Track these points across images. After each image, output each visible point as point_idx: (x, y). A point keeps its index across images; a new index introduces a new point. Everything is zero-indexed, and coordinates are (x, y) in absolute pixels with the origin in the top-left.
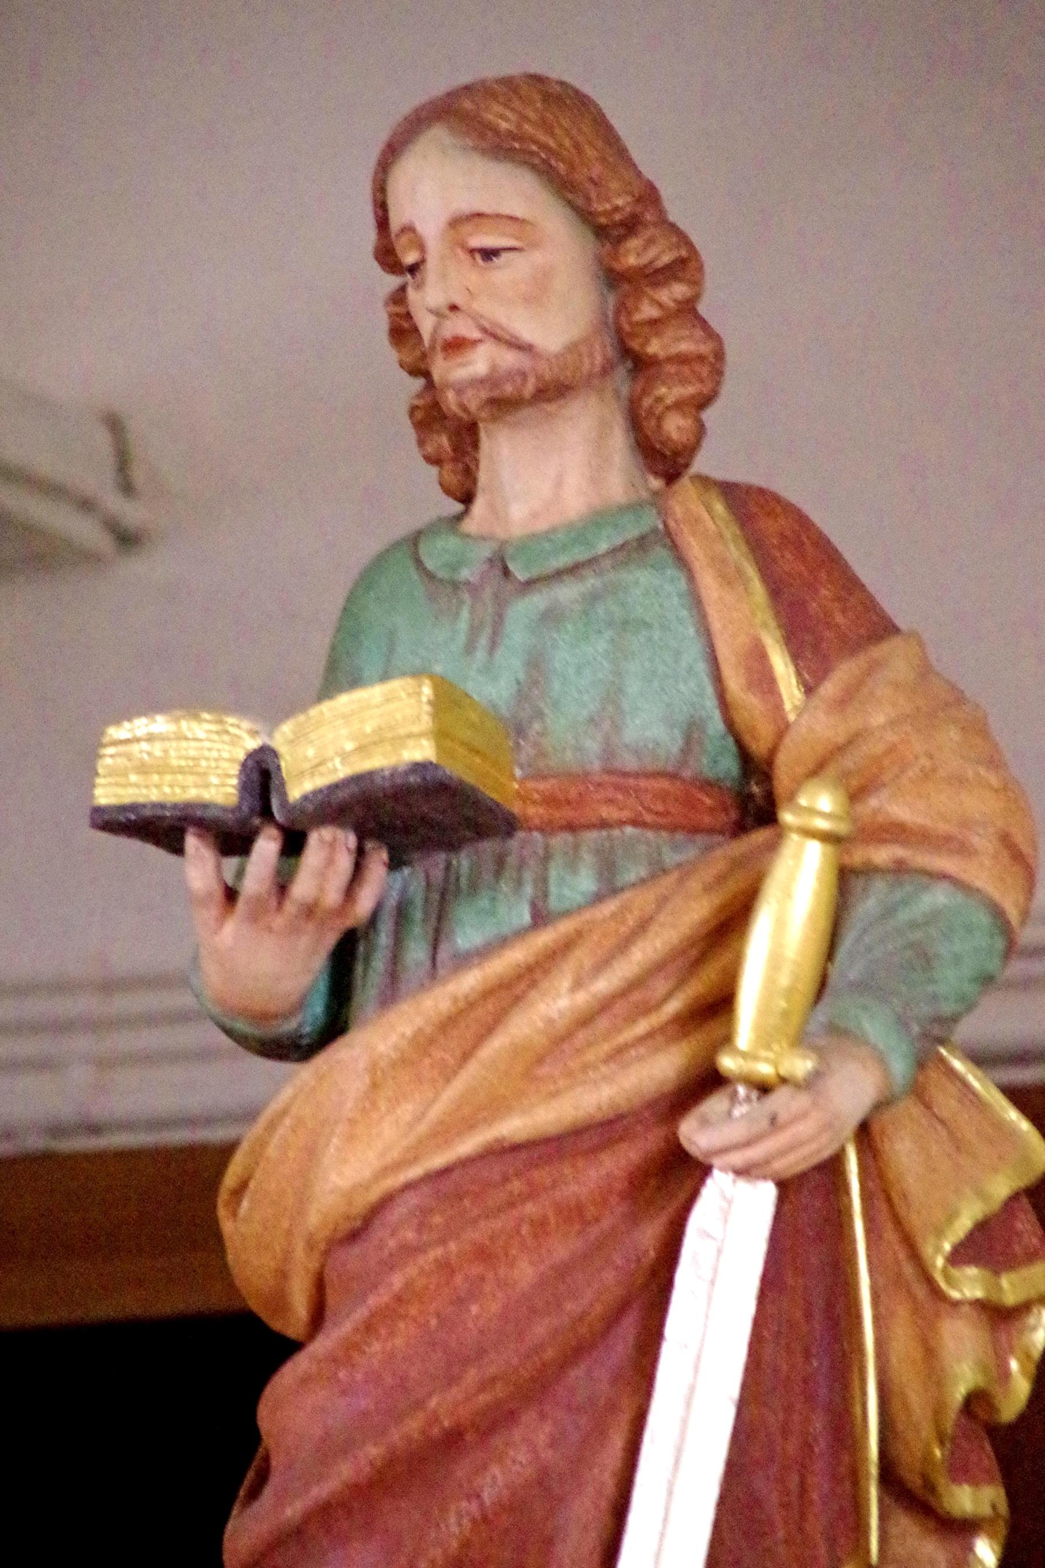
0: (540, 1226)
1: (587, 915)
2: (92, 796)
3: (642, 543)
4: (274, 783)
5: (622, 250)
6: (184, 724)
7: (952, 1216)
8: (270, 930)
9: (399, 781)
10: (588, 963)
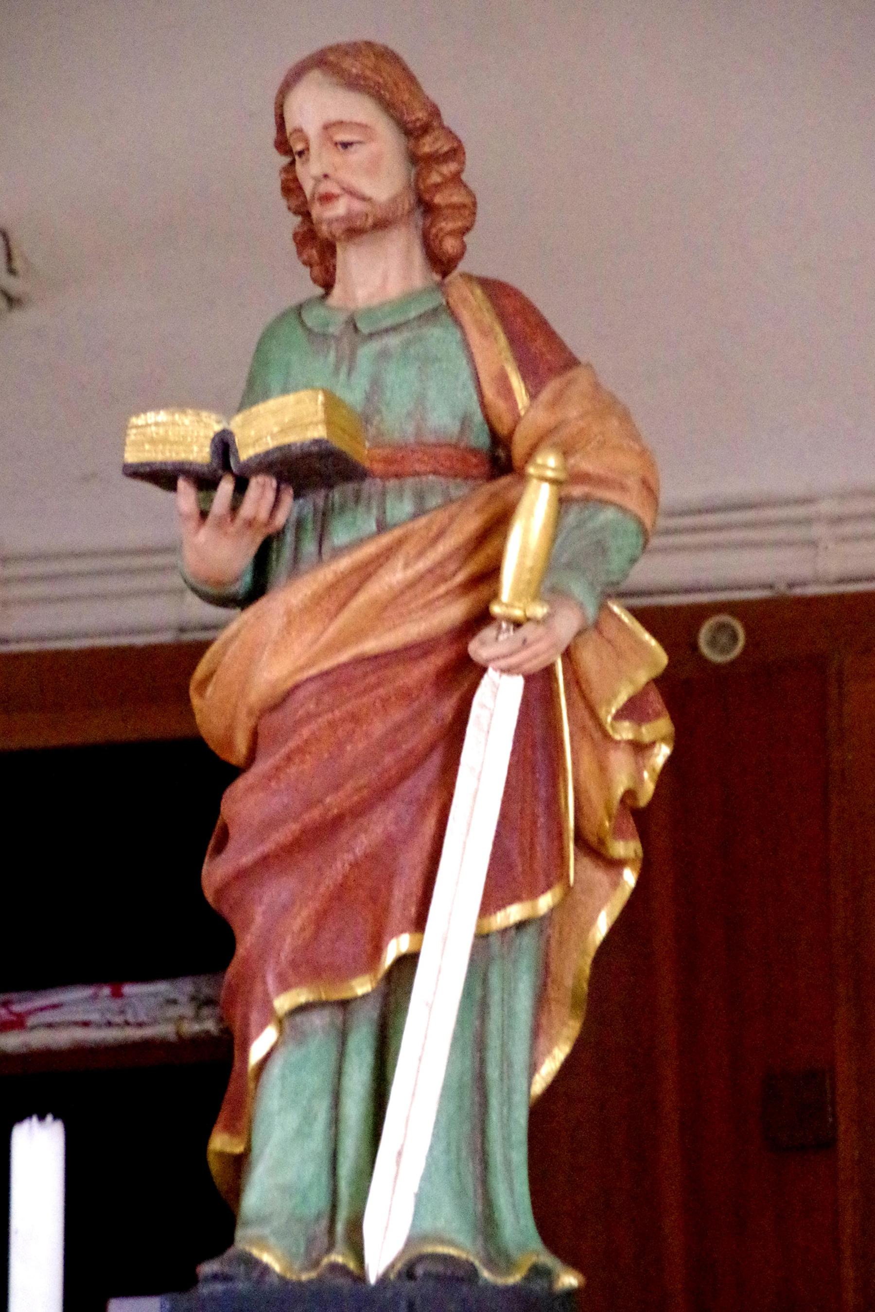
0: (385, 701)
1: (410, 526)
2: (123, 457)
3: (435, 312)
4: (232, 450)
5: (421, 142)
6: (177, 416)
7: (615, 695)
8: (226, 533)
9: (306, 449)
10: (413, 552)
